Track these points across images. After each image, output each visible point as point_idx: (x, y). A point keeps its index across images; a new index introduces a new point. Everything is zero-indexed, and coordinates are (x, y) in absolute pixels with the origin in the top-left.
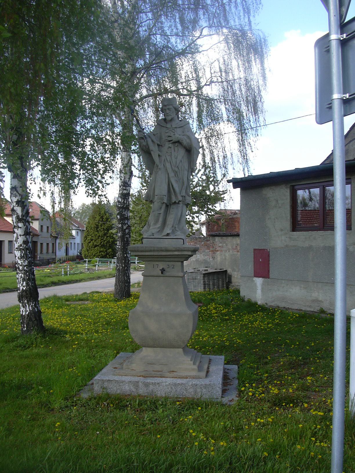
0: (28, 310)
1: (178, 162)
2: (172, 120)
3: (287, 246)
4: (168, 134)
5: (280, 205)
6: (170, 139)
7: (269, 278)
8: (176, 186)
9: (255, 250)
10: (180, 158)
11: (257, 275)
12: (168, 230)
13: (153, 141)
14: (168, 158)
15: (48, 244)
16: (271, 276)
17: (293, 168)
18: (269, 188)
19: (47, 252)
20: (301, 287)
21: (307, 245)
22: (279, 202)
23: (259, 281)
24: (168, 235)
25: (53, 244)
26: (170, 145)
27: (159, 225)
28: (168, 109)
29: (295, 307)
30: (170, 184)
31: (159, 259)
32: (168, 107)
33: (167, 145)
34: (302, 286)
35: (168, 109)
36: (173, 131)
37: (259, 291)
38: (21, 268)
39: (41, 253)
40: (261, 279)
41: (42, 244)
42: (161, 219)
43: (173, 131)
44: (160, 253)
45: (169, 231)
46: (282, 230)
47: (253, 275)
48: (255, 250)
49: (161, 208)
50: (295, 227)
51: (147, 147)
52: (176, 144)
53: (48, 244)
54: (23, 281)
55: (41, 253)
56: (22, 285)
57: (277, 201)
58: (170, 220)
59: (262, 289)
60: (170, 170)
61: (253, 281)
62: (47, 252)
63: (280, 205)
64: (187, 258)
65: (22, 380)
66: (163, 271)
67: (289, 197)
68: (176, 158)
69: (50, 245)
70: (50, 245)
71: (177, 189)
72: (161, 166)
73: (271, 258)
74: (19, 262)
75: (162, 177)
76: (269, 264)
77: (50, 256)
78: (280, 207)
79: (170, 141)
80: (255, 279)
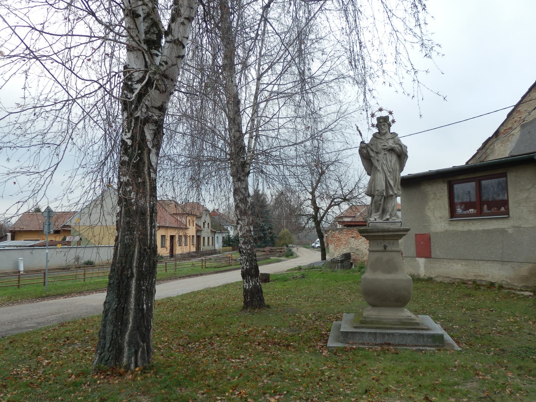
0: (251, 284)
2: (385, 134)
3: (446, 230)
4: (383, 144)
5: (438, 197)
9: (416, 235)
10: (393, 162)
11: (419, 255)
14: (385, 162)
15: (208, 238)
16: (433, 256)
17: (452, 167)
19: (208, 245)
20: (462, 265)
21: (466, 230)
23: (421, 261)
24: (388, 219)
25: (213, 238)
26: (386, 152)
30: (387, 181)
33: (383, 152)
34: (463, 263)
38: (244, 251)
39: (204, 245)
41: (204, 238)
45: (388, 217)
46: (441, 218)
47: (415, 255)
50: (453, 214)
53: (208, 238)
54: (247, 261)
55: (204, 245)
56: (246, 265)
59: (425, 267)
60: (387, 172)
61: (416, 260)
62: (208, 245)
63: (438, 197)
64: (401, 236)
66: (385, 247)
68: (391, 162)
69: (211, 239)
70: (211, 239)
73: (432, 241)
74: (243, 247)
75: (380, 177)
76: (430, 246)
77: (211, 248)
79: (385, 149)
80: (417, 259)
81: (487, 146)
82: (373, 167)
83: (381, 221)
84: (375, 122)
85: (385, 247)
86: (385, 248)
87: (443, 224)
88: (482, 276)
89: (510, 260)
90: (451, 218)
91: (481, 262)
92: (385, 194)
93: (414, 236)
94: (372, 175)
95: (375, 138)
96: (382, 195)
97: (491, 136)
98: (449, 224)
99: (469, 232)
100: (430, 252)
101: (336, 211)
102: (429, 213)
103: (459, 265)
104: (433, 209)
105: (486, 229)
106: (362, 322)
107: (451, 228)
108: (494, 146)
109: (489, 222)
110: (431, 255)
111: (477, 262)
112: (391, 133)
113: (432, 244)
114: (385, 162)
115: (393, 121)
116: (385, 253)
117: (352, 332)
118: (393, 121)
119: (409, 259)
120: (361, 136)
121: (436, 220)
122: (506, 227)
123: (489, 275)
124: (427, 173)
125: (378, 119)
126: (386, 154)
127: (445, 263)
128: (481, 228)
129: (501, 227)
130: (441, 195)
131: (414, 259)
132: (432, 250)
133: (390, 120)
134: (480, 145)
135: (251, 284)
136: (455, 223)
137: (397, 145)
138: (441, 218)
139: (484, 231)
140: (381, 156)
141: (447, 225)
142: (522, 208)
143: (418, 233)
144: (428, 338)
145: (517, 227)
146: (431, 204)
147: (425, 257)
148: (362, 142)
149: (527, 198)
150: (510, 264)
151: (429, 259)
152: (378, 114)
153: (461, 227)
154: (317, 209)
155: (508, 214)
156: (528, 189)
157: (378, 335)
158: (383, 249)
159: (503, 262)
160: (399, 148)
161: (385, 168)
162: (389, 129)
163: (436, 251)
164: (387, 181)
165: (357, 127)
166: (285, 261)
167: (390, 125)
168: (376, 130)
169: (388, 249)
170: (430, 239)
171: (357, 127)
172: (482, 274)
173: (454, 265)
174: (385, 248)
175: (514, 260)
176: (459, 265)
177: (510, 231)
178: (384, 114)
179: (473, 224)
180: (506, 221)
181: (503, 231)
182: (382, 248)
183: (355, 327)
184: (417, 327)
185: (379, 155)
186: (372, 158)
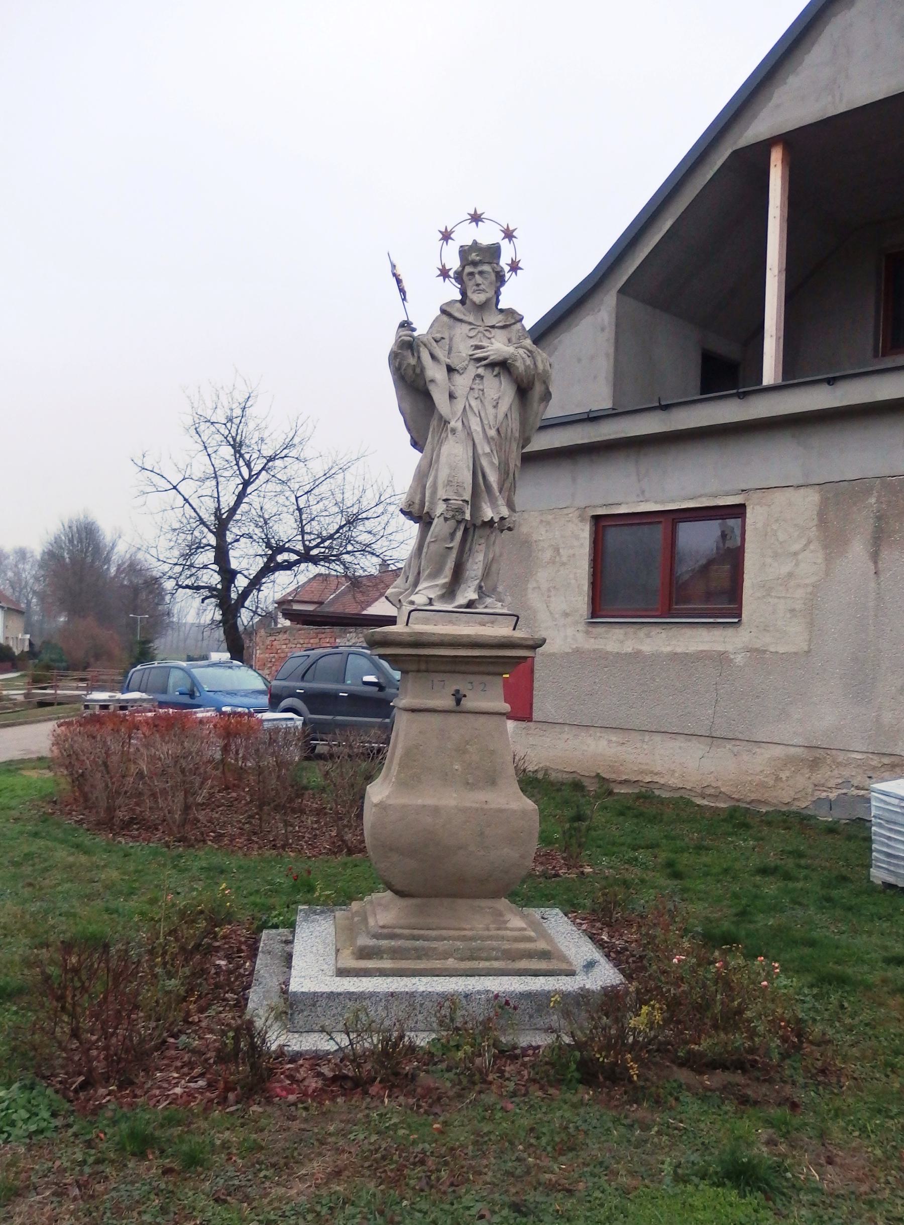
3: (577, 651)
5: (564, 559)
6: (480, 354)
7: (529, 719)
10: (504, 407)
12: (468, 593)
13: (433, 357)
16: (536, 715)
20: (610, 741)
21: (630, 650)
24: (470, 604)
26: (481, 371)
27: (444, 579)
28: (481, 273)
29: (673, 781)
31: (482, 669)
32: (480, 268)
33: (472, 371)
34: (614, 739)
35: (481, 273)
42: (450, 565)
45: (474, 596)
49: (452, 535)
51: (418, 371)
52: (497, 370)
58: (475, 567)
65: (396, 1045)
66: (458, 698)
72: (455, 424)
73: (537, 675)
78: (564, 564)
79: (479, 360)
82: (434, 423)
83: (449, 607)
84: (454, 263)
85: (458, 698)
86: (458, 702)
87: (570, 632)
88: (656, 774)
89: (731, 736)
90: (592, 617)
91: (657, 738)
92: (468, 516)
94: (428, 447)
95: (445, 318)
96: (459, 517)
100: (531, 704)
101: (281, 585)
104: (549, 590)
105: (679, 650)
106: (364, 953)
107: (590, 644)
109: (688, 632)
110: (531, 714)
111: (647, 738)
112: (501, 311)
115: (515, 267)
116: (453, 719)
117: (332, 996)
118: (515, 267)
120: (404, 299)
121: (555, 619)
122: (730, 648)
123: (674, 771)
125: (464, 252)
126: (481, 377)
130: (571, 552)
133: (504, 261)
136: (600, 630)
138: (566, 615)
140: (462, 382)
141: (580, 636)
142: (776, 600)
145: (757, 650)
148: (405, 325)
149: (790, 575)
150: (729, 746)
152: (466, 235)
153: (617, 640)
154: (228, 575)
155: (739, 615)
156: (796, 554)
158: (450, 703)
161: (475, 426)
162: (497, 293)
165: (394, 266)
167: (500, 279)
168: (452, 292)
169: (467, 704)
171: (394, 266)
173: (590, 741)
174: (458, 702)
175: (740, 736)
176: (603, 743)
177: (739, 659)
178: (487, 235)
179: (648, 636)
180: (730, 631)
181: (721, 659)
182: (448, 702)
183: (342, 973)
185: (457, 378)
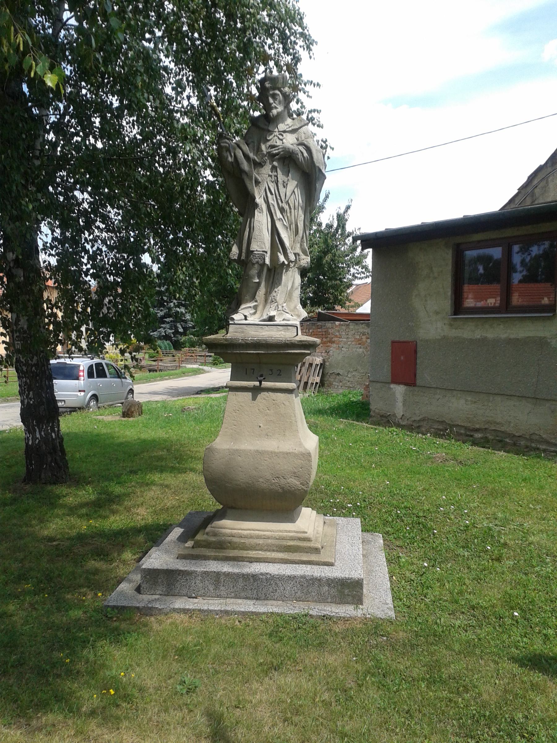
1: (288, 194)
5: (436, 275)
8: (284, 235)
9: (393, 342)
11: (396, 380)
16: (419, 382)
18: (129, 439)
20: (466, 401)
21: (479, 337)
22: (434, 269)
23: (399, 390)
30: (274, 231)
36: (281, 137)
37: (400, 404)
40: (402, 386)
43: (281, 137)
44: (280, 555)
46: (437, 313)
47: (389, 380)
48: (393, 342)
50: (458, 307)
56: (27, 396)
57: (431, 269)
59: (405, 401)
61: (391, 389)
63: (436, 275)
67: (450, 262)
71: (287, 243)
73: (418, 355)
76: (416, 364)
78: (435, 278)
80: (392, 386)
81: (535, 182)
90: (455, 314)
91: (499, 398)
92: (267, 261)
93: (390, 343)
97: (543, 162)
98: (451, 325)
99: (483, 341)
102: (417, 303)
103: (462, 401)
104: (425, 296)
105: (512, 336)
107: (453, 333)
108: (547, 182)
110: (415, 380)
113: (418, 362)
114: (272, 187)
119: (378, 385)
124: (418, 226)
127: (437, 397)
128: (504, 336)
129: (541, 334)
131: (387, 385)
132: (418, 372)
134: (524, 180)
135: (38, 436)
137: (301, 148)
138: (437, 313)
139: (509, 341)
140: (267, 169)
143: (397, 339)
144: (329, 585)
146: (422, 286)
147: (406, 384)
151: (411, 388)
153: (471, 331)
157: (222, 578)
159: (536, 400)
160: (306, 154)
163: (424, 375)
164: (274, 231)
166: (208, 372)
170: (416, 352)
172: (498, 420)
176: (462, 401)
181: (542, 343)
184: (313, 557)
186: (245, 177)
